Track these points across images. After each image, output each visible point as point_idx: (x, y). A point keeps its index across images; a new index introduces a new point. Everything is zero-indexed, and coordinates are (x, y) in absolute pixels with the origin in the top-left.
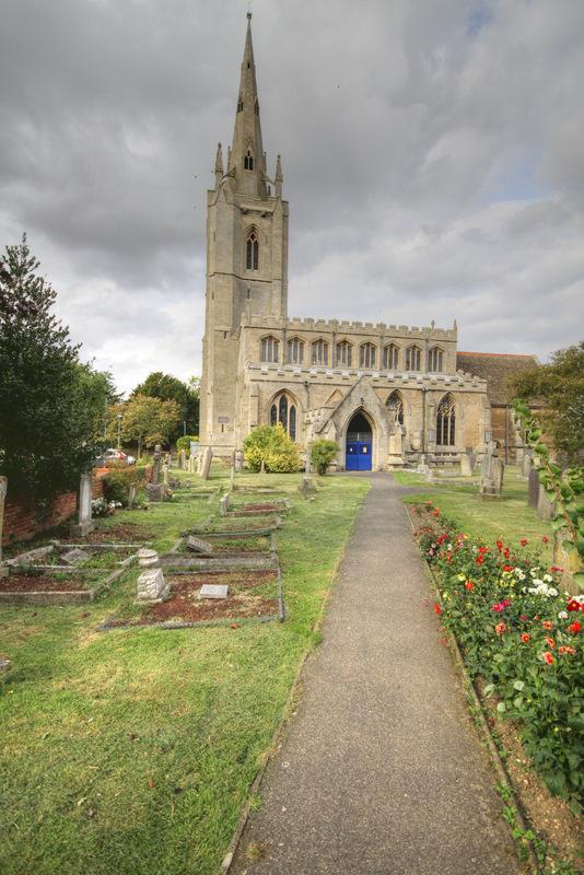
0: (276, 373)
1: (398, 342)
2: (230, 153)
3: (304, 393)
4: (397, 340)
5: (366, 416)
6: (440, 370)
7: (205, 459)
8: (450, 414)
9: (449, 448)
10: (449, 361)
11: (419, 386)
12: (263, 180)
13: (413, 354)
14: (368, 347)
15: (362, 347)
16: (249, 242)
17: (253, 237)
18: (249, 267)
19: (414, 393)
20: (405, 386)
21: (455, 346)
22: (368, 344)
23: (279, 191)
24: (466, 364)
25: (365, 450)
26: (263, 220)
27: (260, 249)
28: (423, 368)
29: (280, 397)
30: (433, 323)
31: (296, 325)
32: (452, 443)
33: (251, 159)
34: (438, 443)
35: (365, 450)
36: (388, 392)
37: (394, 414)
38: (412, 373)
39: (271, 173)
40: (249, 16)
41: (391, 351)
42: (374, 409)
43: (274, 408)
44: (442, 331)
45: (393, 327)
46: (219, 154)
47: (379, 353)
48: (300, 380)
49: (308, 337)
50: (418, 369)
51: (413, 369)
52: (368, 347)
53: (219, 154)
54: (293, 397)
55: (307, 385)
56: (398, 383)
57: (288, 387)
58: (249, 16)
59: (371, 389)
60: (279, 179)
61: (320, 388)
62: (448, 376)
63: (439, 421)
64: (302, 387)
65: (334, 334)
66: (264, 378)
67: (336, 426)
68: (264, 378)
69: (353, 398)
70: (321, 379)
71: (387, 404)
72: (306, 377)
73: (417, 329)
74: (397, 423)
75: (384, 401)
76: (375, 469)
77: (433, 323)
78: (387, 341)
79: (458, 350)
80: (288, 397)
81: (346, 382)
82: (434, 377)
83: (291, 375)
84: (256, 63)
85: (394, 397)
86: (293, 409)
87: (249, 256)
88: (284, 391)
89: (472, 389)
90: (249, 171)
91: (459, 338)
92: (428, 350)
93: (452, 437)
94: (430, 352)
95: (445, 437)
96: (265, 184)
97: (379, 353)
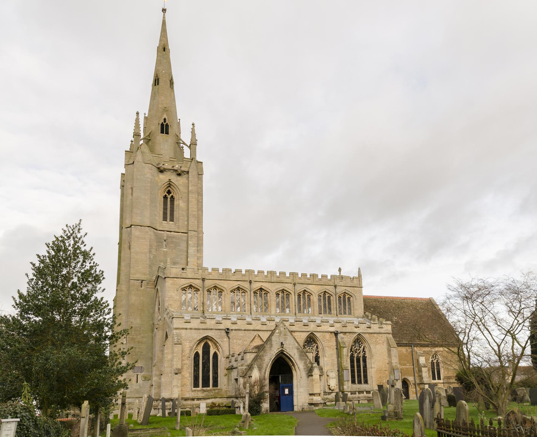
0: (328, 324)
1: (312, 288)
2: (146, 118)
3: (226, 339)
4: (310, 287)
5: (287, 360)
6: (350, 313)
7: (143, 410)
8: (361, 355)
9: (363, 387)
10: (359, 307)
11: (332, 329)
12: (178, 142)
13: (324, 299)
14: (325, 297)
15: (278, 295)
16: (165, 197)
17: (169, 192)
18: (165, 219)
19: (328, 335)
20: (319, 329)
21: (361, 292)
22: (283, 291)
23: (193, 152)
24: (376, 308)
25: (287, 391)
26: (179, 178)
27: (176, 203)
28: (334, 312)
29: (203, 344)
30: (340, 270)
31: (215, 276)
32: (366, 382)
33: (167, 125)
34: (353, 382)
35: (287, 391)
36: (304, 336)
37: (311, 356)
38: (325, 317)
39: (186, 137)
40: (164, 10)
41: (304, 298)
42: (293, 352)
43: (197, 354)
44: (348, 277)
45: (304, 275)
46: (137, 120)
47: (293, 298)
48: (222, 327)
49: (273, 288)
50: (330, 313)
51: (325, 312)
52: (284, 294)
53: (137, 120)
54: (215, 343)
55: (227, 331)
56: (312, 327)
57: (210, 334)
58: (164, 10)
59: (289, 334)
60: (193, 144)
61: (241, 334)
62: (355, 322)
63: (352, 361)
64: (224, 333)
65: (203, 280)
66: (188, 326)
67: (260, 369)
68: (188, 326)
69: (274, 343)
70: (241, 325)
71: (304, 347)
72: (227, 324)
73: (326, 276)
74: (315, 365)
75: (302, 344)
76: (296, 409)
77: (340, 270)
78: (300, 288)
79: (364, 294)
80: (210, 343)
81: (264, 327)
82: (345, 318)
83: (213, 322)
84: (170, 47)
85: (311, 340)
86: (215, 355)
87: (165, 209)
88: (206, 338)
89: (378, 330)
90: (164, 135)
91: (364, 284)
92: (337, 296)
93: (365, 376)
94: (299, 295)
95: (359, 376)
96: (179, 146)
97: (293, 298)
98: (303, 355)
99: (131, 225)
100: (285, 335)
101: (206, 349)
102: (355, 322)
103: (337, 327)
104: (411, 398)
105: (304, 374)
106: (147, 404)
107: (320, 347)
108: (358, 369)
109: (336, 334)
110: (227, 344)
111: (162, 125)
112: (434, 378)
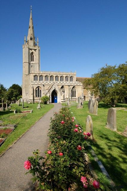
9: (75, 98)
20: (65, 85)
32: (75, 97)
35: (56, 99)
42: (57, 89)
54: (41, 88)
56: (63, 84)
57: (39, 86)
68: (35, 84)
70: (47, 84)
76: (58, 103)
82: (71, 82)
85: (62, 87)
88: (38, 87)
98: (60, 90)
99: (72, 91)
100: (58, 156)
101: (39, 89)
102: (74, 82)
103: (69, 84)
104: (86, 100)
105: (60, 95)
106: (4, 114)
107: (65, 89)
108: (73, 94)
109: (69, 86)
110: (43, 88)
111: (31, 38)
112: (92, 96)
